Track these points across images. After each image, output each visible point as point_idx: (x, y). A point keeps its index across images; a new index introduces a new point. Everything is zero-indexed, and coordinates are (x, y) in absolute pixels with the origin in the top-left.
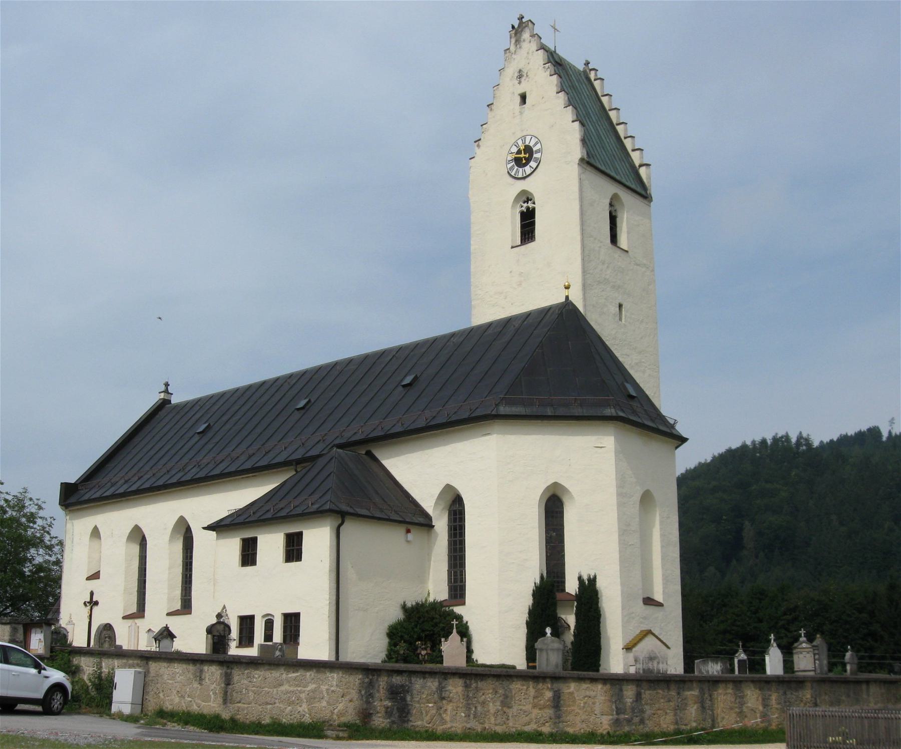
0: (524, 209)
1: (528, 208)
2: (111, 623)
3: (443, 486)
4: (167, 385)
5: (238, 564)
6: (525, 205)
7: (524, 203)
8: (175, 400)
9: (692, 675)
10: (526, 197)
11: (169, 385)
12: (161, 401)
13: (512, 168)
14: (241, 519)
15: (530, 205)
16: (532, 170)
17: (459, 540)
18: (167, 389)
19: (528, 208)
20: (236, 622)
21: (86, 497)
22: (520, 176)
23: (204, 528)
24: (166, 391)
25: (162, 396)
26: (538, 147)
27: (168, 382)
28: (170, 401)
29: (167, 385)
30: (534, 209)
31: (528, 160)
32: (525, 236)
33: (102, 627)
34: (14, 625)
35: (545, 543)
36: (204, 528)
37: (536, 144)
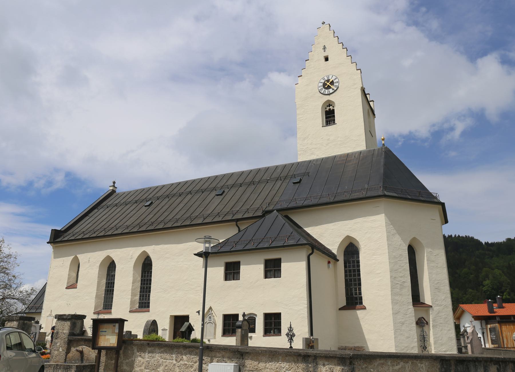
0: (327, 109)
1: (330, 109)
2: (156, 320)
3: (344, 237)
4: (114, 183)
5: (223, 279)
6: (328, 108)
7: (327, 106)
8: (118, 191)
9: (248, 332)
10: (329, 104)
11: (115, 183)
12: (111, 191)
13: (322, 89)
14: (227, 249)
15: (331, 107)
16: (334, 91)
17: (147, 279)
18: (114, 185)
19: (330, 109)
20: (263, 321)
21: (66, 239)
22: (327, 93)
23: (195, 254)
24: (114, 186)
25: (111, 188)
26: (337, 80)
27: (115, 181)
28: (115, 192)
29: (114, 183)
30: (333, 110)
31: (329, 87)
32: (328, 122)
33: (150, 323)
34: (73, 320)
35: (344, 277)
36: (195, 254)
37: (336, 79)
